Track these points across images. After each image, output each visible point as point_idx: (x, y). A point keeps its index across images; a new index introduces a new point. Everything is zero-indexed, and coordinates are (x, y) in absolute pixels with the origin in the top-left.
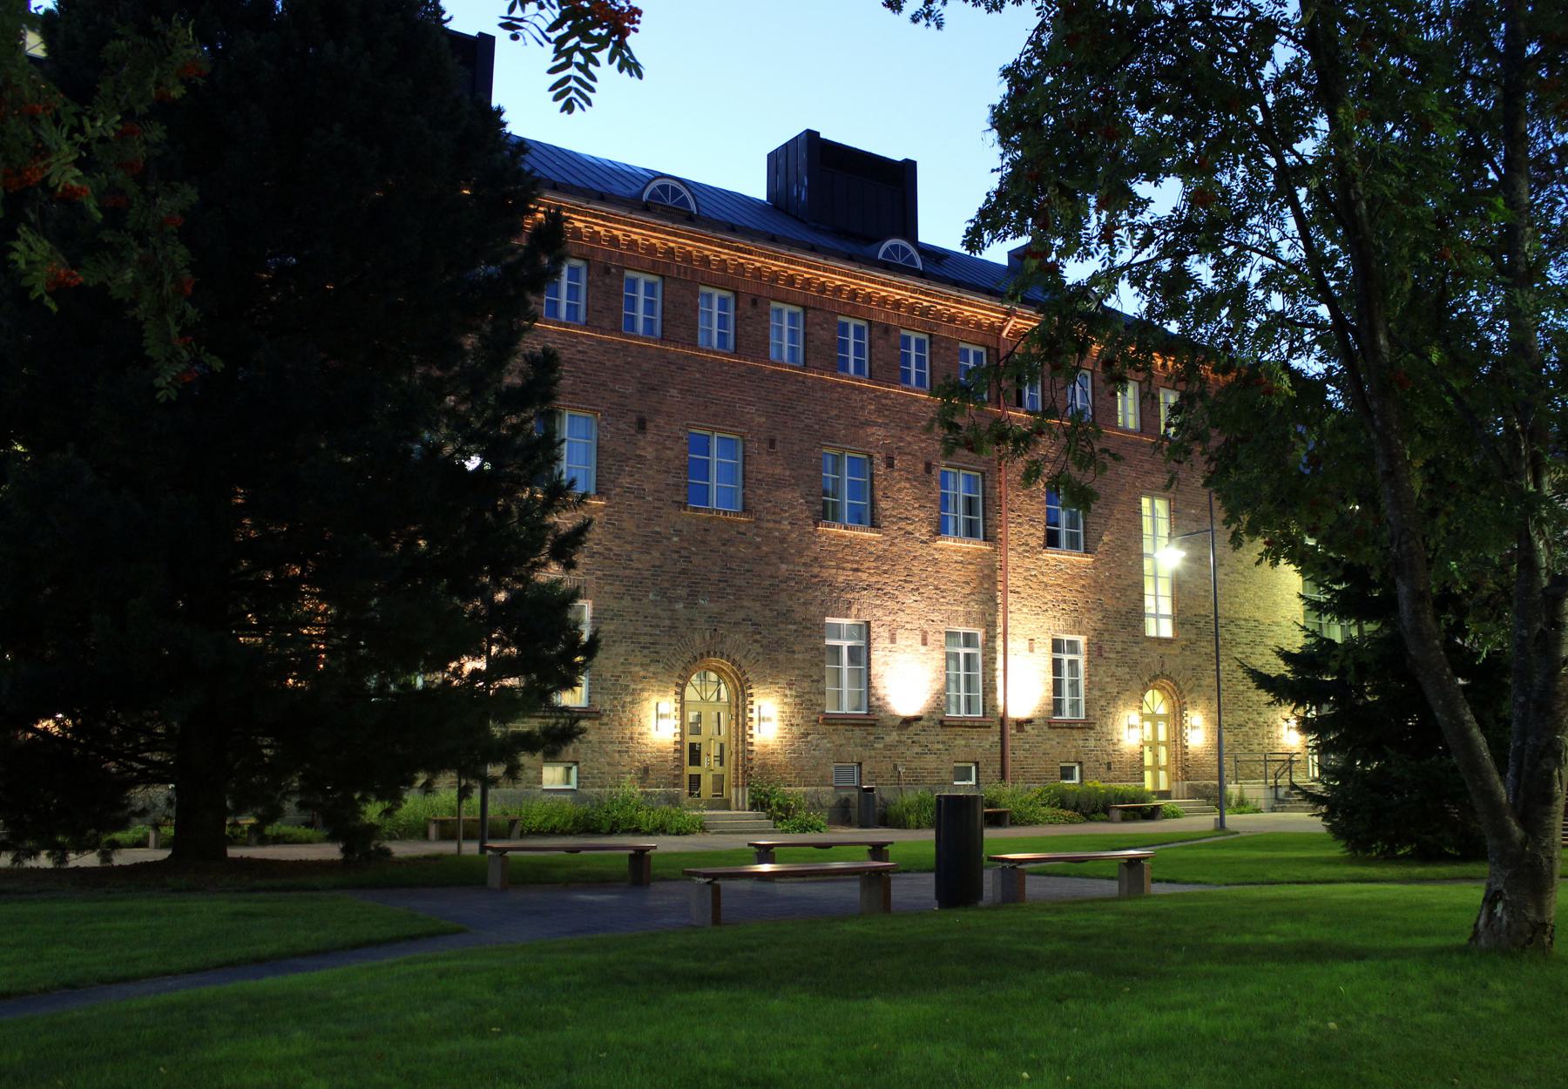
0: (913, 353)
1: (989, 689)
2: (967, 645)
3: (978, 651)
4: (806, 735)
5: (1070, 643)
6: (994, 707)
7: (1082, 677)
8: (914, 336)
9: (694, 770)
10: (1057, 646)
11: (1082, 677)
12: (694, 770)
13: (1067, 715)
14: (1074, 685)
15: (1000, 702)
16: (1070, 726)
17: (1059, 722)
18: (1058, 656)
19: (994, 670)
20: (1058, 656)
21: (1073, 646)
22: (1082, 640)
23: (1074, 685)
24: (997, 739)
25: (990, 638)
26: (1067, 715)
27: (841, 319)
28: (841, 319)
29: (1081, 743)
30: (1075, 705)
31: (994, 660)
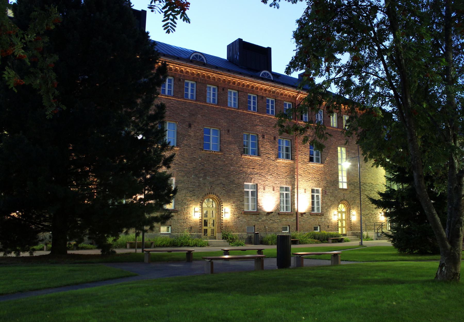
0: (270, 104)
1: (293, 204)
2: (286, 191)
3: (289, 193)
4: (238, 217)
5: (317, 190)
6: (294, 209)
7: (320, 200)
8: (270, 99)
9: (205, 228)
10: (313, 191)
11: (320, 200)
12: (205, 228)
13: (316, 211)
14: (318, 203)
15: (296, 208)
16: (317, 215)
17: (314, 213)
18: (313, 194)
19: (294, 198)
20: (313, 194)
21: (317, 191)
22: (320, 189)
23: (318, 203)
24: (295, 218)
25: (293, 189)
26: (316, 211)
27: (249, 94)
28: (249, 94)
29: (320, 220)
30: (318, 208)
31: (294, 195)
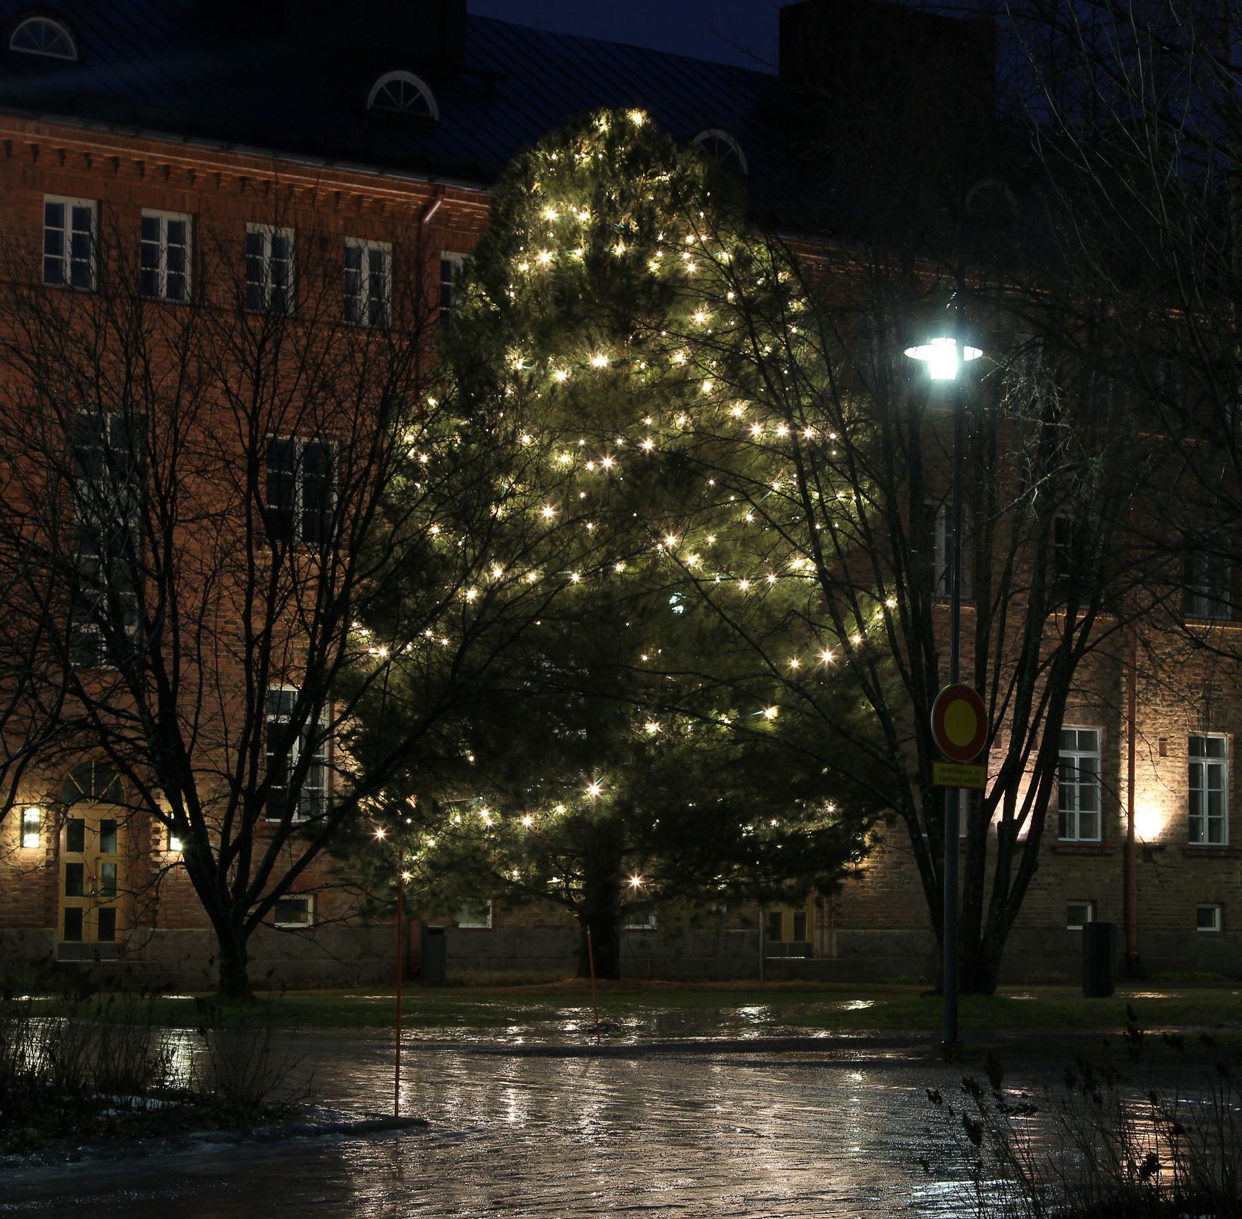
0: (163, 243)
1: (1112, 804)
2: (1082, 748)
3: (1096, 755)
4: (898, 864)
5: (1210, 741)
6: (1118, 828)
7: (1225, 788)
8: (165, 218)
9: (74, 902)
10: (1195, 747)
11: (1225, 788)
12: (74, 902)
13: (1204, 840)
14: (1214, 800)
15: (1125, 822)
16: (1211, 853)
17: (1068, 844)
18: (1194, 760)
19: (1118, 780)
20: (1194, 760)
21: (1214, 748)
22: (1225, 738)
23: (1214, 800)
24: (1119, 871)
25: (1113, 739)
26: (1204, 840)
27: (49, 198)
28: (147, 213)
29: (1223, 877)
30: (1214, 825)
31: (1117, 767)
